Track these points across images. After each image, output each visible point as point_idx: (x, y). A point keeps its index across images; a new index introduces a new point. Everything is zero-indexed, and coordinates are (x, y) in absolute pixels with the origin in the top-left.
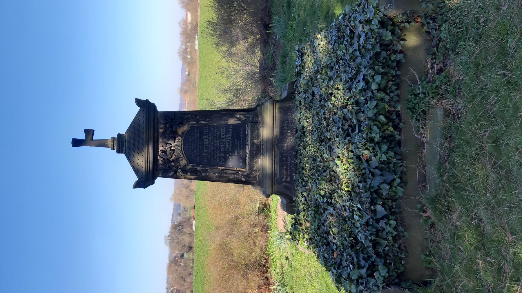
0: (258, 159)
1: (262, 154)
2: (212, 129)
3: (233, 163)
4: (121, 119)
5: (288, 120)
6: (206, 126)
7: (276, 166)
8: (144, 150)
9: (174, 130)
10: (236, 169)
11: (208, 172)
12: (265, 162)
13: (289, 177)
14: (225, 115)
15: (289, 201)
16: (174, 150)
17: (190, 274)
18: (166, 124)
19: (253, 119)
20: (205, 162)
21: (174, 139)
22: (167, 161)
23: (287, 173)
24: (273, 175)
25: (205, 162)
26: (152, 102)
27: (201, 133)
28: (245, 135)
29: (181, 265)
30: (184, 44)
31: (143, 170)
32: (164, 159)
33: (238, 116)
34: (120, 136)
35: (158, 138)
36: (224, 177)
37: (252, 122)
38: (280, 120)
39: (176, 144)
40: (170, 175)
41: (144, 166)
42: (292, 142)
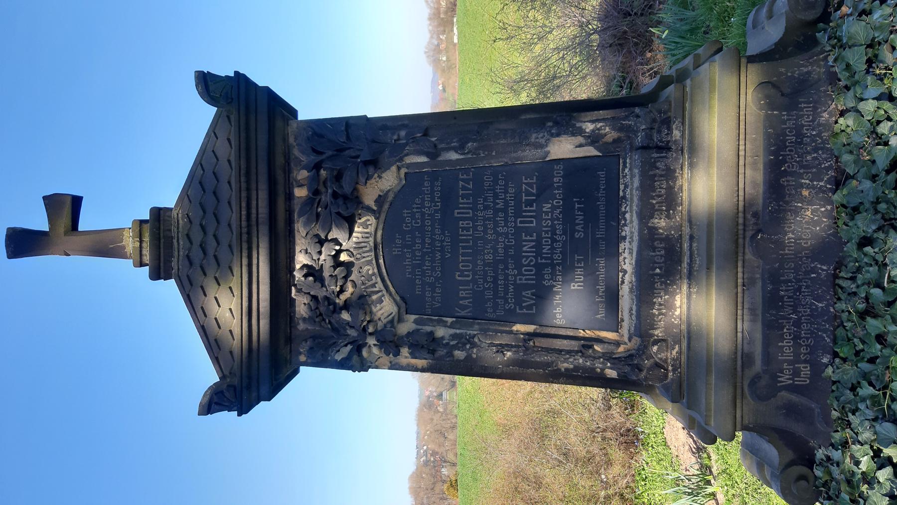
0: (673, 295)
1: (690, 276)
2: (488, 180)
3: (569, 307)
4: (158, 157)
5: (800, 135)
6: (466, 171)
7: (744, 325)
8: (236, 270)
9: (347, 189)
10: (581, 333)
11: (474, 345)
12: (702, 310)
13: (805, 370)
14: (539, 125)
15: (790, 455)
16: (348, 266)
17: (454, 427)
18: (317, 167)
19: (649, 137)
20: (464, 308)
21: (350, 223)
22: (326, 308)
23: (797, 355)
24: (741, 359)
25: (464, 308)
26: (261, 83)
27: (448, 199)
28: (615, 203)
29: (439, 412)
30: (435, 36)
31: (236, 344)
32: (314, 298)
33: (589, 127)
34: (158, 214)
35: (290, 223)
36: (537, 365)
37: (644, 148)
38: (767, 136)
39: (357, 239)
40: (339, 357)
41: (236, 331)
42: (816, 223)
